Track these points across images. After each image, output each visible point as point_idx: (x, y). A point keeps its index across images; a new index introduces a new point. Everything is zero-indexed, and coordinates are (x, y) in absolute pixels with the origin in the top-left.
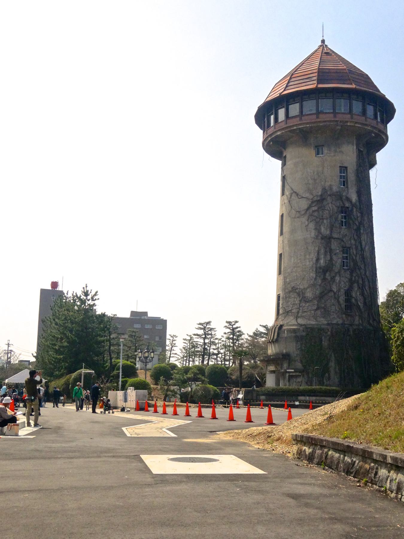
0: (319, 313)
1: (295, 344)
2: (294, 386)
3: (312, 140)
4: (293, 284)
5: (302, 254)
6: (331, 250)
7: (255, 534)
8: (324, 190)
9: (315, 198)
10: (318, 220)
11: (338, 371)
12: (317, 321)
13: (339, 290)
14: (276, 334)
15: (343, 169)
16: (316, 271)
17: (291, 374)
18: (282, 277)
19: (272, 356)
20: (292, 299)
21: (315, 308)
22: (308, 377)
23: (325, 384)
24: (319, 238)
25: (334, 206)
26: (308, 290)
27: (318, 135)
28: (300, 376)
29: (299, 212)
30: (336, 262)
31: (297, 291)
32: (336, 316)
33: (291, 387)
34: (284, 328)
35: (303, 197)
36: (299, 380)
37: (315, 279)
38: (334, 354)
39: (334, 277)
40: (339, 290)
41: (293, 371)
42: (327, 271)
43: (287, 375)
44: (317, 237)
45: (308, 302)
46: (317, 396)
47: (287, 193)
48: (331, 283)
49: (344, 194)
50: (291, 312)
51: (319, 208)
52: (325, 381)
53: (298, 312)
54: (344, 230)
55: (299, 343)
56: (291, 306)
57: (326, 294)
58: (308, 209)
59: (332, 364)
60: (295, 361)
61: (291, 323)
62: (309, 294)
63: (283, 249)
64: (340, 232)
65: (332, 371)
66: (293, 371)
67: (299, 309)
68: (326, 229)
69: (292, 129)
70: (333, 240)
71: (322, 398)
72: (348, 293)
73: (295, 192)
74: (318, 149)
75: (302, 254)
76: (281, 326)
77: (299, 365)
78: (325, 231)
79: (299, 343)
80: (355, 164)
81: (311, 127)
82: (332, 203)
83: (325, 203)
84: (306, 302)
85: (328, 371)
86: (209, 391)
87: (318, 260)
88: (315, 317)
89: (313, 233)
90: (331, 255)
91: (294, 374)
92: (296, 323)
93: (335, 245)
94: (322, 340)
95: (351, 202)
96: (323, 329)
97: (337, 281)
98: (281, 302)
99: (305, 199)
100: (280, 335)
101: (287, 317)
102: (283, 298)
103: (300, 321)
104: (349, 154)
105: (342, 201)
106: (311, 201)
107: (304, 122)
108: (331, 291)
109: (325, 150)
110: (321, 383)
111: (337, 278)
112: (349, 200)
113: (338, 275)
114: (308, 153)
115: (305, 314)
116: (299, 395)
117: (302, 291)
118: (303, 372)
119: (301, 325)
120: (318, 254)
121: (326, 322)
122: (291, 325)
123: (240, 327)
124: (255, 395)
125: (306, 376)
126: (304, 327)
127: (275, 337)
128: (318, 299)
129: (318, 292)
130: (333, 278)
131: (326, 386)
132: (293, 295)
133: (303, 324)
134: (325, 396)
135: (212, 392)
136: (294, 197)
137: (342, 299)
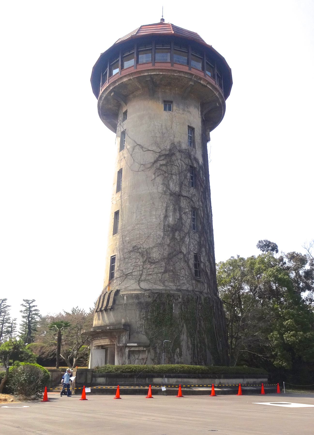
0: (167, 276)
1: (138, 313)
2: (136, 364)
3: (160, 95)
6: (180, 209)
8: (173, 144)
9: (164, 152)
10: (167, 175)
11: (190, 346)
13: (189, 253)
14: (111, 300)
15: (191, 129)
16: (164, 229)
18: (118, 236)
19: (109, 326)
20: (134, 261)
21: (163, 271)
22: (156, 353)
23: (176, 361)
24: (168, 193)
25: (183, 164)
26: (155, 250)
27: (167, 91)
29: (144, 165)
30: (186, 222)
31: (140, 250)
32: (185, 282)
33: (131, 365)
34: (121, 293)
35: (149, 150)
36: (141, 356)
37: (163, 238)
38: (187, 326)
39: (184, 237)
40: (189, 253)
41: (136, 345)
42: (176, 230)
43: (127, 350)
44: (165, 192)
45: (154, 263)
46: (179, 377)
47: (128, 146)
48: (181, 243)
49: (192, 153)
51: (167, 163)
52: (176, 357)
53: (141, 275)
54: (193, 191)
55: (144, 311)
56: (132, 268)
57: (175, 256)
58: (155, 162)
59: (184, 337)
60: (138, 333)
61: (130, 287)
62: (155, 255)
63: (121, 205)
64: (189, 191)
65: (184, 344)
66: (136, 345)
67: (142, 271)
68: (175, 186)
69: (142, 75)
70: (182, 198)
71: (185, 380)
72: (196, 257)
73: (139, 145)
74: (168, 105)
76: (118, 292)
77: (144, 338)
78: (174, 187)
79: (144, 311)
80: (200, 128)
81: (164, 76)
82: (181, 160)
83: (174, 158)
84: (151, 263)
85: (180, 347)
86: (38, 373)
87: (166, 217)
88: (163, 281)
89: (161, 188)
90: (180, 214)
91: (137, 349)
92: (138, 288)
93: (184, 203)
94: (172, 308)
95: (199, 164)
96: (173, 295)
97: (187, 242)
98: (116, 264)
100: (117, 302)
101: (125, 282)
102: (120, 260)
103: (144, 285)
104: (195, 117)
105: (191, 159)
106: (158, 154)
107: (157, 68)
108: (181, 252)
109: (174, 107)
110: (171, 360)
111: (187, 240)
112: (196, 160)
113: (187, 237)
114: (155, 107)
115: (151, 277)
116: (153, 377)
117: (146, 251)
118: (149, 346)
119: (146, 290)
120: (166, 211)
121: (174, 288)
122: (131, 290)
123: (36, 306)
124: (89, 376)
125: (152, 351)
126: (149, 292)
127: (111, 304)
128: (166, 260)
129: (166, 254)
130: (182, 239)
131: (178, 363)
132: (133, 255)
133: (147, 288)
134: (189, 377)
135: (41, 375)
136: (137, 149)
137: (192, 262)
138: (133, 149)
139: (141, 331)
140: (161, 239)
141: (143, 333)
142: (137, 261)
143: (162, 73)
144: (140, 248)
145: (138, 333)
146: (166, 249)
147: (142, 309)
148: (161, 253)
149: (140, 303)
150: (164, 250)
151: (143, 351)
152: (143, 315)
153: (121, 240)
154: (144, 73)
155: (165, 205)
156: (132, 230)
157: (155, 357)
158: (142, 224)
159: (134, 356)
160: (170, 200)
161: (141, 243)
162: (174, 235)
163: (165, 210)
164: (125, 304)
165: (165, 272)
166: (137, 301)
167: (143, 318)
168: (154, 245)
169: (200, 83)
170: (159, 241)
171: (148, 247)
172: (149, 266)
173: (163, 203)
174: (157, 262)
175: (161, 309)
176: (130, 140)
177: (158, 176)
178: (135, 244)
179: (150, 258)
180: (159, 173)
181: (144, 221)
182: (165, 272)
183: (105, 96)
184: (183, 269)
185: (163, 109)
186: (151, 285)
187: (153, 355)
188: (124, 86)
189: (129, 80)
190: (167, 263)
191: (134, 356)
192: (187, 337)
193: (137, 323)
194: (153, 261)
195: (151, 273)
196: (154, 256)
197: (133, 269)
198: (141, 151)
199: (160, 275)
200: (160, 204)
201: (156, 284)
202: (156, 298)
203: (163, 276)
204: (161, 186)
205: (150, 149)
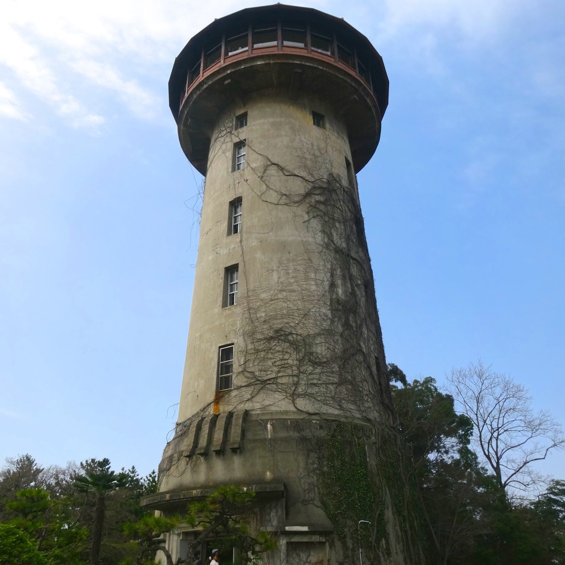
4: (278, 325)
5: (299, 268)
7: (93, 498)
12: (341, 408)
16: (331, 305)
17: (295, 539)
19: (248, 484)
22: (345, 547)
28: (322, 544)
30: (360, 300)
31: (290, 338)
35: (296, 175)
43: (283, 542)
50: (277, 384)
53: (296, 384)
55: (313, 456)
56: (276, 369)
59: (389, 514)
60: (305, 502)
66: (305, 529)
68: (340, 238)
69: (291, 61)
75: (300, 268)
77: (319, 515)
79: (313, 456)
84: (315, 364)
87: (333, 285)
91: (305, 539)
98: (237, 361)
99: (300, 179)
100: (249, 435)
103: (303, 404)
108: (361, 350)
115: (315, 390)
125: (338, 544)
129: (339, 349)
138: (265, 171)
139: (313, 500)
140: (329, 322)
141: (316, 503)
142: (286, 357)
143: (321, 68)
144: (291, 334)
145: (305, 502)
146: (337, 340)
147: (309, 451)
148: (331, 347)
149: (303, 440)
150: (335, 342)
151: (322, 544)
152: (313, 463)
153: (247, 315)
154: (294, 60)
155: (329, 267)
156: (272, 300)
157: (346, 557)
158: (293, 291)
159: (298, 555)
160: (335, 259)
161: (292, 324)
162: (347, 319)
163: (329, 274)
164: (270, 439)
165: (339, 384)
166: (296, 435)
167: (315, 470)
168: (317, 331)
169: (366, 101)
170: (326, 324)
171: (305, 333)
172: (311, 368)
173: (326, 263)
174: (325, 362)
175: (347, 454)
176: (256, 156)
177: (314, 217)
178: (280, 326)
179: (311, 354)
180: (315, 214)
181: (295, 287)
182: (339, 384)
183: (210, 83)
184: (366, 381)
185: (312, 122)
186: (317, 406)
187: (341, 553)
188: (253, 71)
189: (266, 64)
190: (342, 367)
191: (298, 555)
192: (393, 514)
193: (303, 481)
194: (317, 361)
195: (315, 381)
196: (319, 352)
197: (279, 372)
198: (282, 174)
199: (331, 387)
200: (321, 263)
201: (326, 404)
202: (335, 430)
203: (338, 390)
204: (320, 234)
205: (297, 174)
